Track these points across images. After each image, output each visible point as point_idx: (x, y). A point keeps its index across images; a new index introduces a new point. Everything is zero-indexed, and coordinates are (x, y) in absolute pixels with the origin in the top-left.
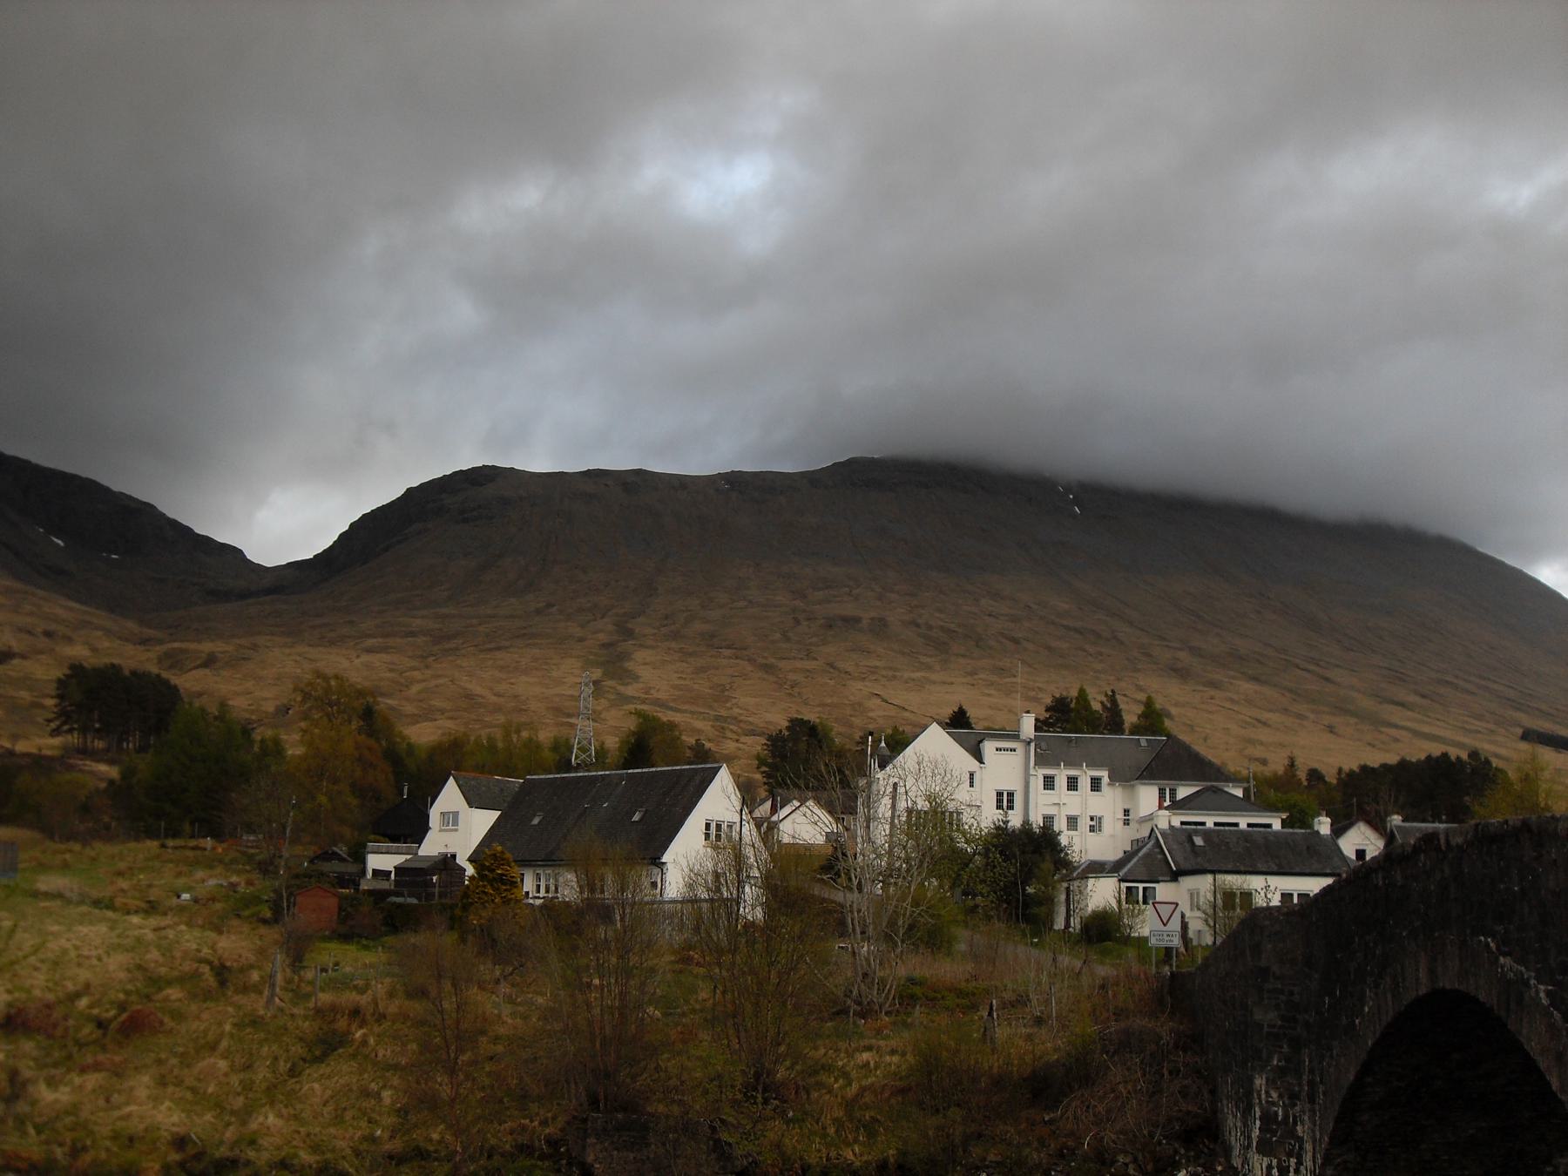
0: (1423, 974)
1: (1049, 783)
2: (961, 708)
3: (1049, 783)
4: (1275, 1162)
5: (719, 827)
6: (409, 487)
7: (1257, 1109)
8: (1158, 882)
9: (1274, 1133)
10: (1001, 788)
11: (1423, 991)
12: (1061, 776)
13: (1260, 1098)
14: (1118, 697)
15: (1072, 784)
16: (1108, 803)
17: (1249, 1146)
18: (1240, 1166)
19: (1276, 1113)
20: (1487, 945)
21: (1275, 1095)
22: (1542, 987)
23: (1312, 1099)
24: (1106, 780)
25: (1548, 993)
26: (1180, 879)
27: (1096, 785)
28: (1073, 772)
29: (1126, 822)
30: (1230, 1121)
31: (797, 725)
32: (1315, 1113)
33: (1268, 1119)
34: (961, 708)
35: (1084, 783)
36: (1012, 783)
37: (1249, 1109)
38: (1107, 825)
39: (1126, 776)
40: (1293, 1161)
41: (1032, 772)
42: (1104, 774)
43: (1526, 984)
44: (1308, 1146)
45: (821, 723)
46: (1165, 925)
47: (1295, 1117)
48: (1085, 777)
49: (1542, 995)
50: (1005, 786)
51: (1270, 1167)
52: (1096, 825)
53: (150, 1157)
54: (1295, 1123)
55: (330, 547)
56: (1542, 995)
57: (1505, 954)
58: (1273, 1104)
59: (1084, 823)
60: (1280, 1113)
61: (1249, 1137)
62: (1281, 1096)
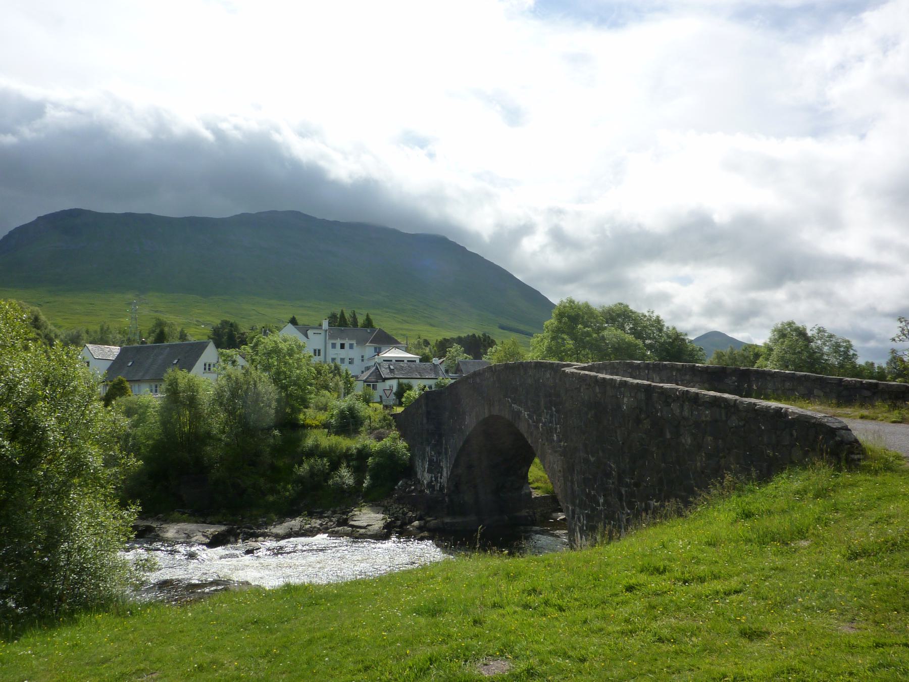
0: (486, 411)
1: (334, 346)
2: (294, 317)
3: (334, 346)
4: (433, 475)
5: (209, 365)
6: (39, 216)
7: (427, 458)
8: (378, 382)
9: (433, 466)
10: (315, 348)
11: (487, 416)
12: (338, 342)
13: (428, 455)
14: (356, 315)
15: (342, 346)
16: (355, 353)
17: (424, 470)
18: (421, 478)
19: (434, 459)
20: (508, 401)
21: (433, 453)
22: (526, 413)
23: (446, 453)
24: (355, 345)
25: (528, 414)
26: (386, 381)
27: (351, 346)
28: (342, 342)
29: (363, 360)
30: (417, 463)
31: (225, 323)
32: (447, 458)
33: (431, 461)
34: (294, 317)
35: (347, 346)
36: (319, 345)
37: (424, 458)
38: (355, 362)
39: (361, 342)
40: (439, 474)
41: (327, 342)
42: (354, 342)
43: (521, 412)
44: (445, 470)
45: (234, 322)
46: (388, 397)
47: (440, 460)
48: (347, 343)
49: (526, 415)
50: (317, 347)
51: (432, 477)
52: (351, 362)
53: (423, 653)
54: (440, 462)
55: (459, 245)
56: (526, 415)
57: (514, 404)
58: (433, 456)
59: (347, 361)
60: (435, 459)
61: (424, 468)
62: (435, 453)
